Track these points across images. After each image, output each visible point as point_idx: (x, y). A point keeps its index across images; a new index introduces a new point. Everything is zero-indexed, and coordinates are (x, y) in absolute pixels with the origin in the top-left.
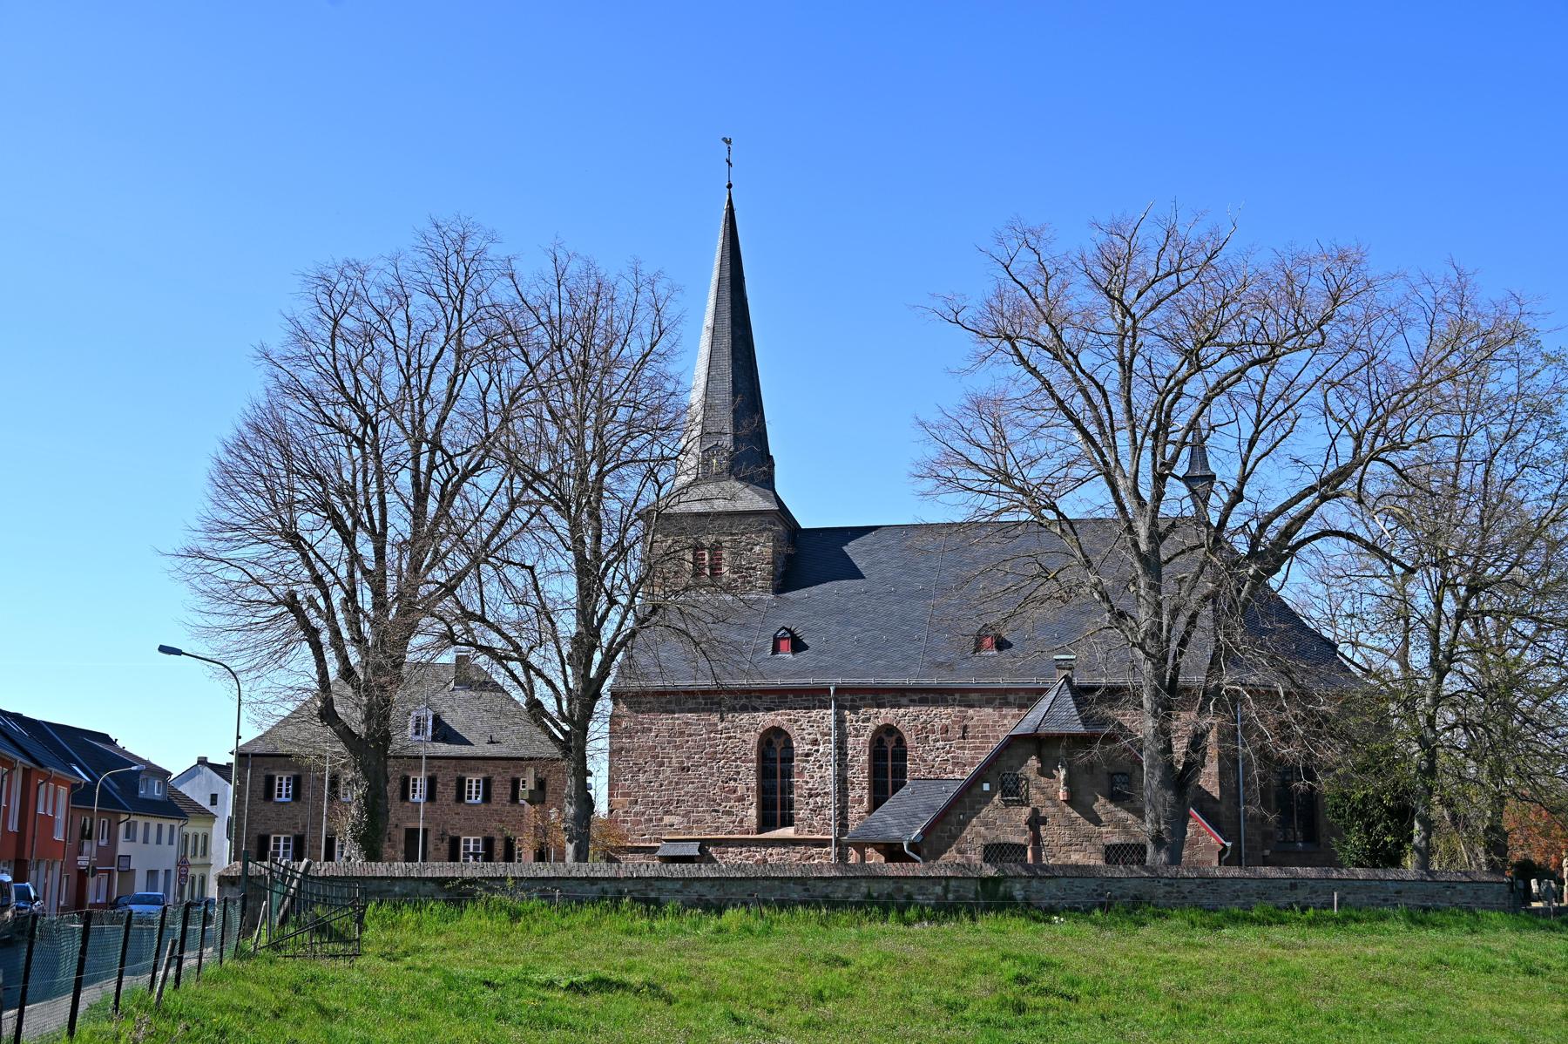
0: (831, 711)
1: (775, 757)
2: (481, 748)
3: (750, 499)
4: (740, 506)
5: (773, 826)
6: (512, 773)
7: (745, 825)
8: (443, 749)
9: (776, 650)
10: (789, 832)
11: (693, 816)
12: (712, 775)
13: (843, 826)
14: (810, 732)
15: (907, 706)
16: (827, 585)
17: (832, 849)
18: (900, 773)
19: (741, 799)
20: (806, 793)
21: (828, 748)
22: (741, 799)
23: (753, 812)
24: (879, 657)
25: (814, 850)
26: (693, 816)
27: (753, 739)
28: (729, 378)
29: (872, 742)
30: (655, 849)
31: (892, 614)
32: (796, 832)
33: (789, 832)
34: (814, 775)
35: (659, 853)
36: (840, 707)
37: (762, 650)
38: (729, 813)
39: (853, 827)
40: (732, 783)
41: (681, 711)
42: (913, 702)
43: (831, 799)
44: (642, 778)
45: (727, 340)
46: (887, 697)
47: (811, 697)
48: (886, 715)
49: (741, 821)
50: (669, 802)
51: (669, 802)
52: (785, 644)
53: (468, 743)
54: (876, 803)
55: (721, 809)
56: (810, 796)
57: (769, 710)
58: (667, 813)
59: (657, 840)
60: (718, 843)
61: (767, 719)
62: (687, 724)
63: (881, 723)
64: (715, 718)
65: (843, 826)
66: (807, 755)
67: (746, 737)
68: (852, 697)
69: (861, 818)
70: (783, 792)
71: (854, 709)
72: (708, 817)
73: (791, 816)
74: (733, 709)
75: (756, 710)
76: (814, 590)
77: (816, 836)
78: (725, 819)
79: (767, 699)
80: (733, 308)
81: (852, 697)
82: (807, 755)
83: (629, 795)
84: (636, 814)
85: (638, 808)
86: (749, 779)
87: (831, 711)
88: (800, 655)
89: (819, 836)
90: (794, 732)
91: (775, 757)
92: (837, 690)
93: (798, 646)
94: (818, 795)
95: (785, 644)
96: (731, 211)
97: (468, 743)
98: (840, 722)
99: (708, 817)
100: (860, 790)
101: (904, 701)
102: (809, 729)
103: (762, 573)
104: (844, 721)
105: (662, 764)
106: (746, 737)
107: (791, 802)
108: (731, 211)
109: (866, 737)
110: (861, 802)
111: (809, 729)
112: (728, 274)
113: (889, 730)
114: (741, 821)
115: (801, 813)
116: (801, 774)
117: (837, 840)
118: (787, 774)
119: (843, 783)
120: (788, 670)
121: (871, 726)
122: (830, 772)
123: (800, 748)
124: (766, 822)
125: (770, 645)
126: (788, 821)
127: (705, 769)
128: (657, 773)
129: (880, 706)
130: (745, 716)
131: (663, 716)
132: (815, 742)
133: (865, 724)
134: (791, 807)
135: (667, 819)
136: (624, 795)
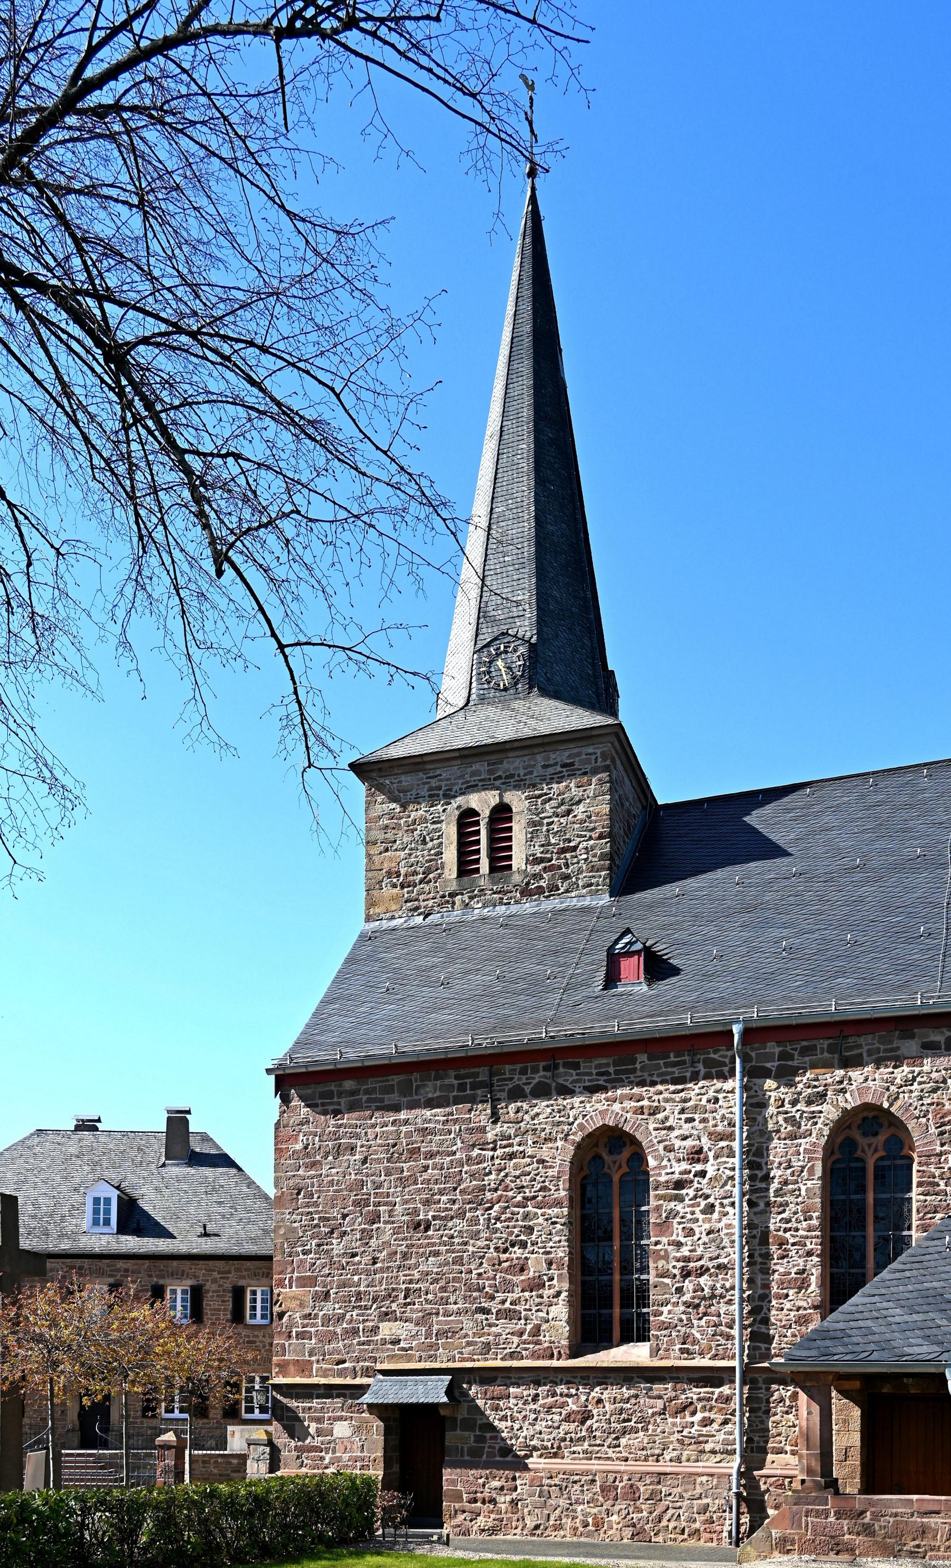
0: (734, 1083)
1: (608, 1181)
2: (187, 1242)
3: (557, 717)
4: (544, 728)
5: (604, 1341)
6: (233, 1279)
7: (545, 1339)
8: (131, 1243)
9: (612, 979)
10: (635, 1354)
11: (438, 1323)
12: (476, 1235)
13: (760, 1338)
14: (685, 1133)
15: (916, 1060)
16: (719, 874)
17: (735, 1391)
18: (896, 1216)
19: (536, 1285)
20: (675, 1267)
21: (726, 1167)
22: (536, 1285)
23: (560, 1310)
24: (842, 973)
25: (694, 1393)
26: (438, 1323)
27: (560, 1155)
28: (529, 513)
29: (829, 1149)
30: (363, 1389)
31: (861, 900)
32: (655, 1352)
33: (635, 1354)
34: (693, 1231)
35: (367, 1398)
36: (754, 1073)
37: (587, 984)
38: (510, 1315)
39: (784, 1339)
40: (517, 1252)
41: (411, 1106)
42: (931, 1048)
43: (734, 1279)
44: (337, 1247)
45: (525, 447)
46: (867, 1042)
47: (685, 1053)
48: (866, 1084)
49: (537, 1331)
50: (390, 1295)
51: (390, 1295)
52: (631, 967)
53: (171, 1236)
54: (838, 1290)
55: (494, 1306)
56: (686, 1274)
57: (593, 1090)
58: (386, 1316)
59: (368, 1372)
60: (487, 1376)
61: (592, 1111)
62: (424, 1131)
63: (851, 1101)
64: (481, 1114)
65: (760, 1338)
66: (679, 1185)
67: (545, 1152)
68: (784, 1046)
69: (803, 1321)
70: (626, 1302)
71: (786, 1075)
72: (468, 1324)
73: (644, 1319)
74: (516, 1094)
75: (566, 1092)
76: (692, 883)
77: (698, 1362)
78: (503, 1327)
79: (590, 1067)
80: (538, 387)
81: (784, 1046)
82: (679, 1185)
83: (312, 1281)
84: (327, 1320)
85: (329, 1308)
86: (550, 1242)
87: (734, 1083)
88: (663, 986)
89: (706, 1362)
90: (648, 1134)
91: (608, 1181)
92: (747, 1033)
93: (657, 968)
94: (703, 1271)
95: (631, 967)
96: (533, 200)
97: (171, 1236)
98: (755, 1105)
99: (468, 1324)
100: (800, 1259)
101: (911, 1046)
102: (684, 1127)
103: (592, 849)
104: (764, 1105)
105: (375, 1218)
106: (545, 1152)
107: (644, 1288)
108: (533, 200)
109: (817, 1136)
110: (802, 1285)
111: (684, 1127)
112: (528, 328)
113: (871, 1121)
114: (537, 1331)
115: (666, 1311)
116: (664, 1226)
117: (747, 1370)
118: (636, 1226)
119: (758, 1240)
120: (639, 1006)
121: (829, 1112)
122: (732, 1220)
123: (663, 1167)
124: (591, 1331)
125: (601, 975)
126: (636, 1331)
127: (461, 1224)
128: (366, 1235)
129: (848, 1063)
130: (542, 1106)
131: (378, 1118)
132: (697, 1155)
133: (813, 1107)
134: (644, 1300)
135: (387, 1329)
136: (304, 1282)
